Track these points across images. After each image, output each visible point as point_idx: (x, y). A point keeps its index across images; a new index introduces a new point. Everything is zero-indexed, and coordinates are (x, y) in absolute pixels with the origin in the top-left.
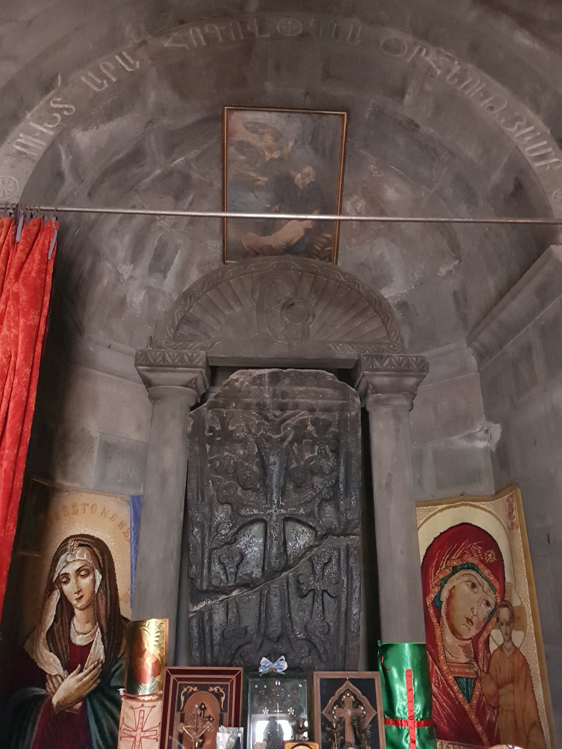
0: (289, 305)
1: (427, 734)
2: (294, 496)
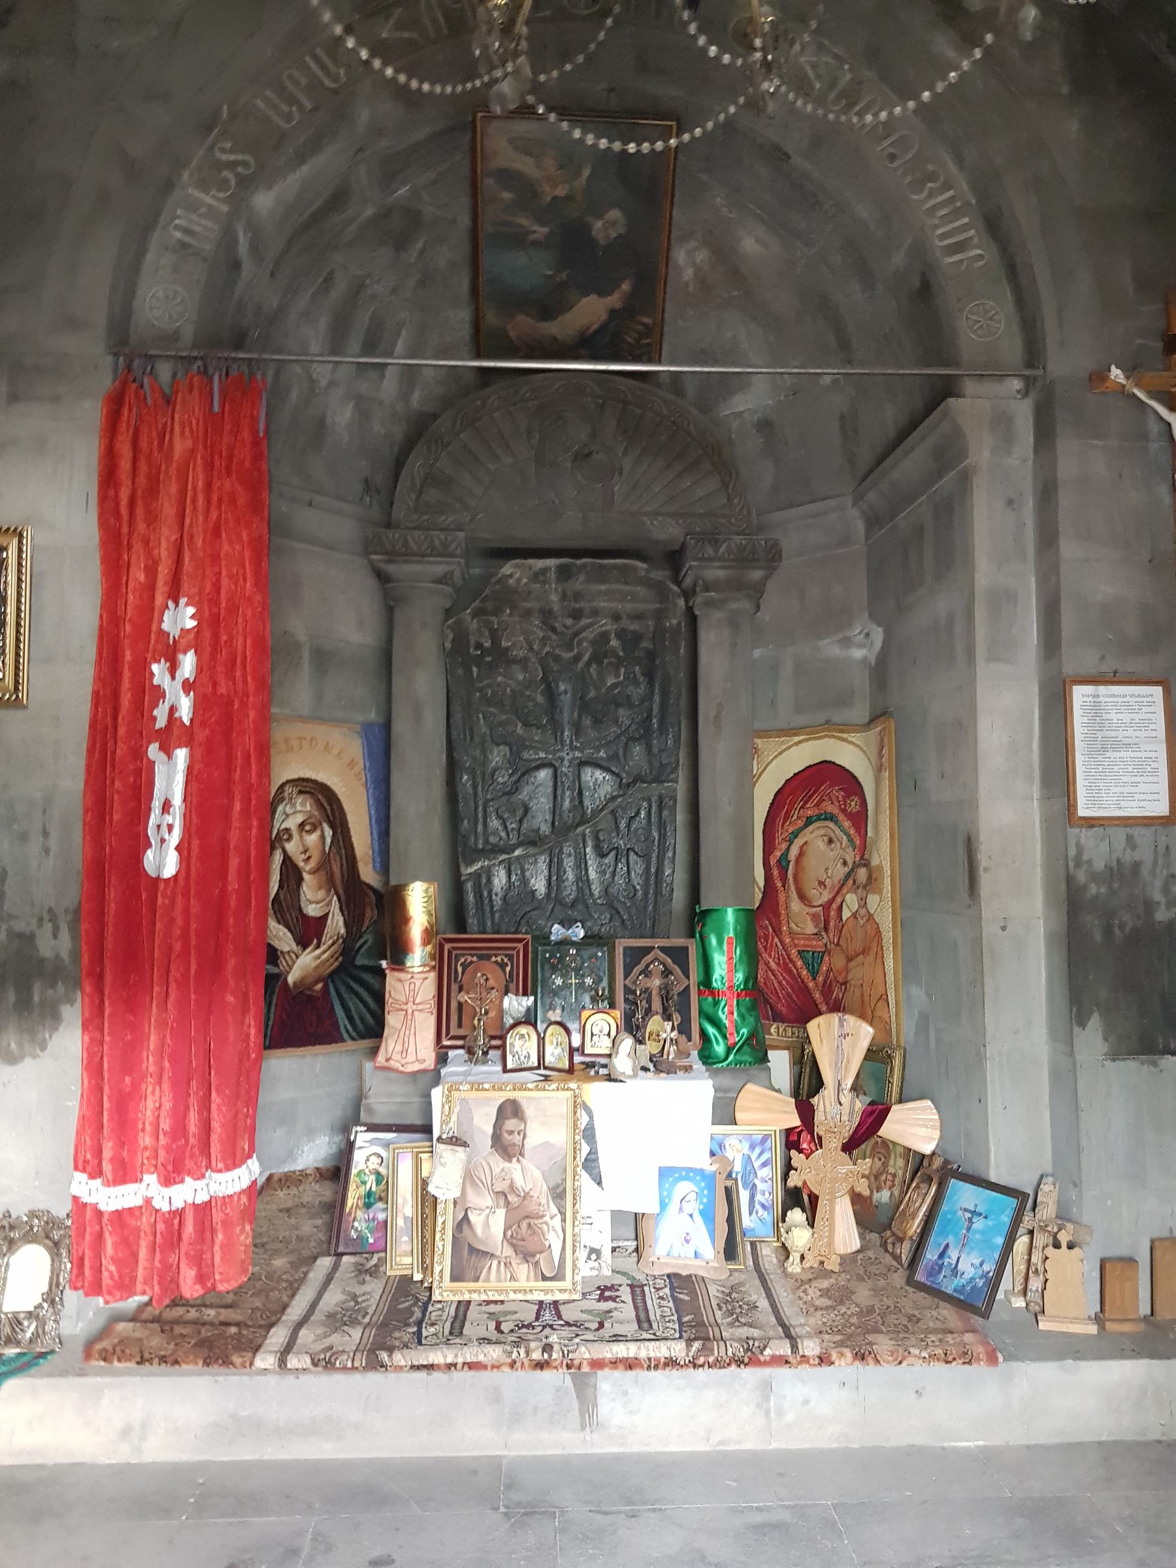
0: (583, 456)
1: (749, 1005)
2: (593, 734)
